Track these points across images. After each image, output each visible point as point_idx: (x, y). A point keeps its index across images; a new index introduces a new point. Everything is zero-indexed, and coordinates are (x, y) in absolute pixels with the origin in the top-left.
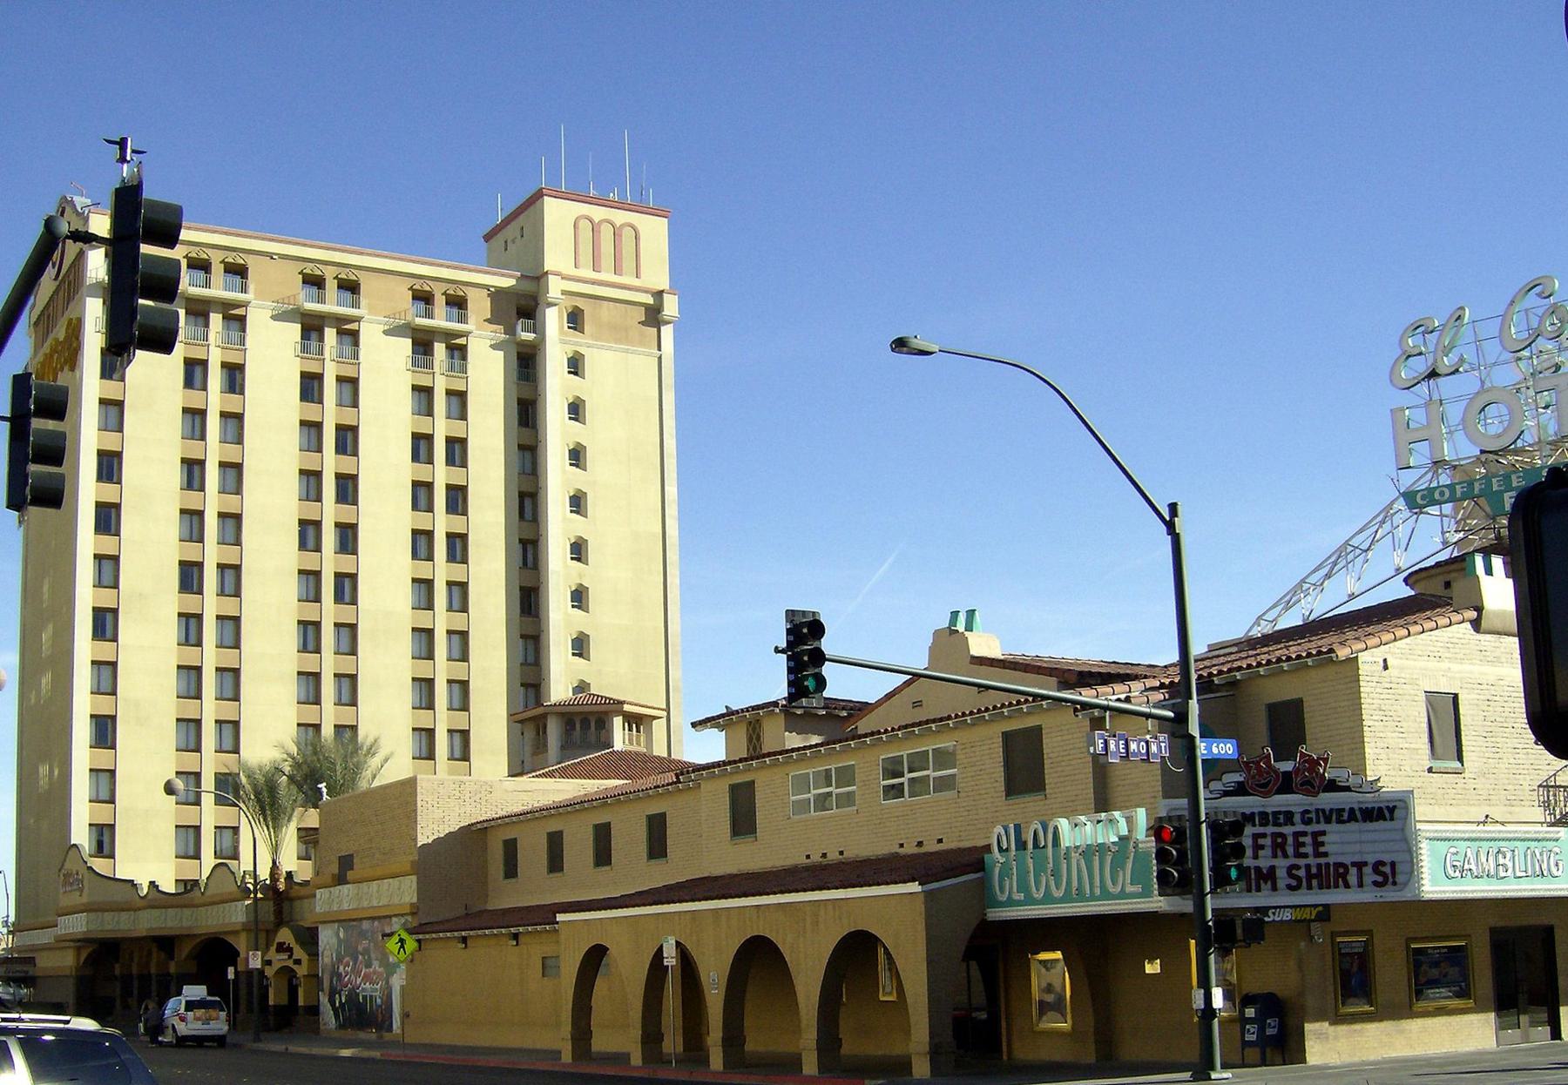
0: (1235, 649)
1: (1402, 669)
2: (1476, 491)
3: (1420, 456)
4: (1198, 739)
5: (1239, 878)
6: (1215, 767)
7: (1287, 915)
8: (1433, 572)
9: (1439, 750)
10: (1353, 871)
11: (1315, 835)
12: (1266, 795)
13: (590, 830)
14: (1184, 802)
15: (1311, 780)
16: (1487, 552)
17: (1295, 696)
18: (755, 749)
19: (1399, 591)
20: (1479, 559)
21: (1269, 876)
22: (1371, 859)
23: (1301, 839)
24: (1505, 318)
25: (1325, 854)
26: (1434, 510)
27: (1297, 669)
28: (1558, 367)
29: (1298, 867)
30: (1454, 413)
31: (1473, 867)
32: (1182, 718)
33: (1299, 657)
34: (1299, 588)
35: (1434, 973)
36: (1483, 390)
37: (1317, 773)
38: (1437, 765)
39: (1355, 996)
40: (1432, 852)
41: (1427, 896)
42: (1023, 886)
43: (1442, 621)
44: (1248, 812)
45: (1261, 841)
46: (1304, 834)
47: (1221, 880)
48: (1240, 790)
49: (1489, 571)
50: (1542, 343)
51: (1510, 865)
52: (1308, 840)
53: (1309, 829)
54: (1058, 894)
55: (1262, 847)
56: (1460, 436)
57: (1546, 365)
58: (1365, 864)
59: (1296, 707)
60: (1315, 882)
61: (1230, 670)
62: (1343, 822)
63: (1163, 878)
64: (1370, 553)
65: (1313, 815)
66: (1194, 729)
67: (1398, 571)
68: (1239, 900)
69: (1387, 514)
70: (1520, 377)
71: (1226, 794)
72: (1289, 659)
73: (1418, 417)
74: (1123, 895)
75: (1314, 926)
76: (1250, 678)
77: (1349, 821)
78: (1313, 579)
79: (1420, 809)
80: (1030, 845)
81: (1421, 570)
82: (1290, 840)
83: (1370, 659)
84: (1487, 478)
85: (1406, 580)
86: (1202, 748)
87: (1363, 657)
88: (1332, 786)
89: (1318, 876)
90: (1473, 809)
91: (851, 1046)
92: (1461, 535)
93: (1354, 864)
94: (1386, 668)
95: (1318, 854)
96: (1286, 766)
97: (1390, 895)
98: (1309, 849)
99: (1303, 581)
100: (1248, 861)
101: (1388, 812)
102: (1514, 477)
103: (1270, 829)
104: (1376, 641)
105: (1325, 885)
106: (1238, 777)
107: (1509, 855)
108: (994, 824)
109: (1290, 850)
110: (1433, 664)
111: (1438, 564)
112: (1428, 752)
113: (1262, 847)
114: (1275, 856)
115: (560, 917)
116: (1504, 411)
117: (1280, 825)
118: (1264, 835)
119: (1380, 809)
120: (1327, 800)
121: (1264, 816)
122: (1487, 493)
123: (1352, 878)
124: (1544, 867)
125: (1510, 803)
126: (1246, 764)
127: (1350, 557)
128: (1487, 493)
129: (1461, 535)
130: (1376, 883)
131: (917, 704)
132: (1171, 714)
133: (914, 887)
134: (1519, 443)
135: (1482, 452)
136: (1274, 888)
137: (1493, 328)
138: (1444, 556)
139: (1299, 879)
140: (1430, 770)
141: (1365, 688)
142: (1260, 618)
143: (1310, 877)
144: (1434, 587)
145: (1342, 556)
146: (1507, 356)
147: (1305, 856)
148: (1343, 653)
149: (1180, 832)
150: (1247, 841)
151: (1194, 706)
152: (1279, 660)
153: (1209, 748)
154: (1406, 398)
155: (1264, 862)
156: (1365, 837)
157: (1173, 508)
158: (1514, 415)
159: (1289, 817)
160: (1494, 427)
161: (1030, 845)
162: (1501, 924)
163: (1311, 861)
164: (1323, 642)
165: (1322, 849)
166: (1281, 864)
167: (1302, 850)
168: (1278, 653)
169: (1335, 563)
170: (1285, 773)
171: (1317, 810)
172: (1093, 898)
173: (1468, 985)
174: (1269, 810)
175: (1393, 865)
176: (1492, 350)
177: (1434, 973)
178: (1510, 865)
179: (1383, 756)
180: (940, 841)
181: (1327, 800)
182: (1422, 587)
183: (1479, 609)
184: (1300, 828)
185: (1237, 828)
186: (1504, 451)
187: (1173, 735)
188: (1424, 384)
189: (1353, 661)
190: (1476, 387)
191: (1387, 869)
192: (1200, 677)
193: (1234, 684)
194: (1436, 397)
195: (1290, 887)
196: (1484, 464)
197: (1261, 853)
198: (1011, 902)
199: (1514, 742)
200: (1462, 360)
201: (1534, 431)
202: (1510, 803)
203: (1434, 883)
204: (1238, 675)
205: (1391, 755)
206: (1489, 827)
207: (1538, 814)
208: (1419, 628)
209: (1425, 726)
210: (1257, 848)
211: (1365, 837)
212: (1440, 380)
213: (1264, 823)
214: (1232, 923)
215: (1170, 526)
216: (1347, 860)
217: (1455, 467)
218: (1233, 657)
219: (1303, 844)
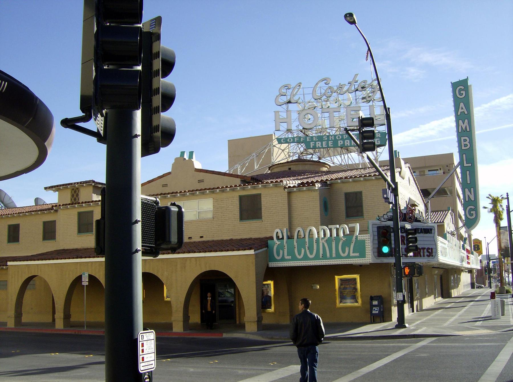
2: (302, 141)
3: (284, 127)
13: (7, 227)
18: (75, 199)
42: (291, 252)
54: (311, 257)
58: (425, 248)
74: (348, 257)
80: (296, 237)
91: (75, 318)
108: (277, 228)
115: (9, 263)
120: (416, 225)
130: (427, 256)
131: (165, 185)
133: (252, 252)
135: (303, 128)
138: (285, 161)
154: (279, 108)
156: (425, 239)
161: (296, 237)
172: (331, 258)
175: (432, 249)
180: (202, 237)
181: (416, 225)
191: (430, 251)
198: (283, 259)
211: (425, 239)
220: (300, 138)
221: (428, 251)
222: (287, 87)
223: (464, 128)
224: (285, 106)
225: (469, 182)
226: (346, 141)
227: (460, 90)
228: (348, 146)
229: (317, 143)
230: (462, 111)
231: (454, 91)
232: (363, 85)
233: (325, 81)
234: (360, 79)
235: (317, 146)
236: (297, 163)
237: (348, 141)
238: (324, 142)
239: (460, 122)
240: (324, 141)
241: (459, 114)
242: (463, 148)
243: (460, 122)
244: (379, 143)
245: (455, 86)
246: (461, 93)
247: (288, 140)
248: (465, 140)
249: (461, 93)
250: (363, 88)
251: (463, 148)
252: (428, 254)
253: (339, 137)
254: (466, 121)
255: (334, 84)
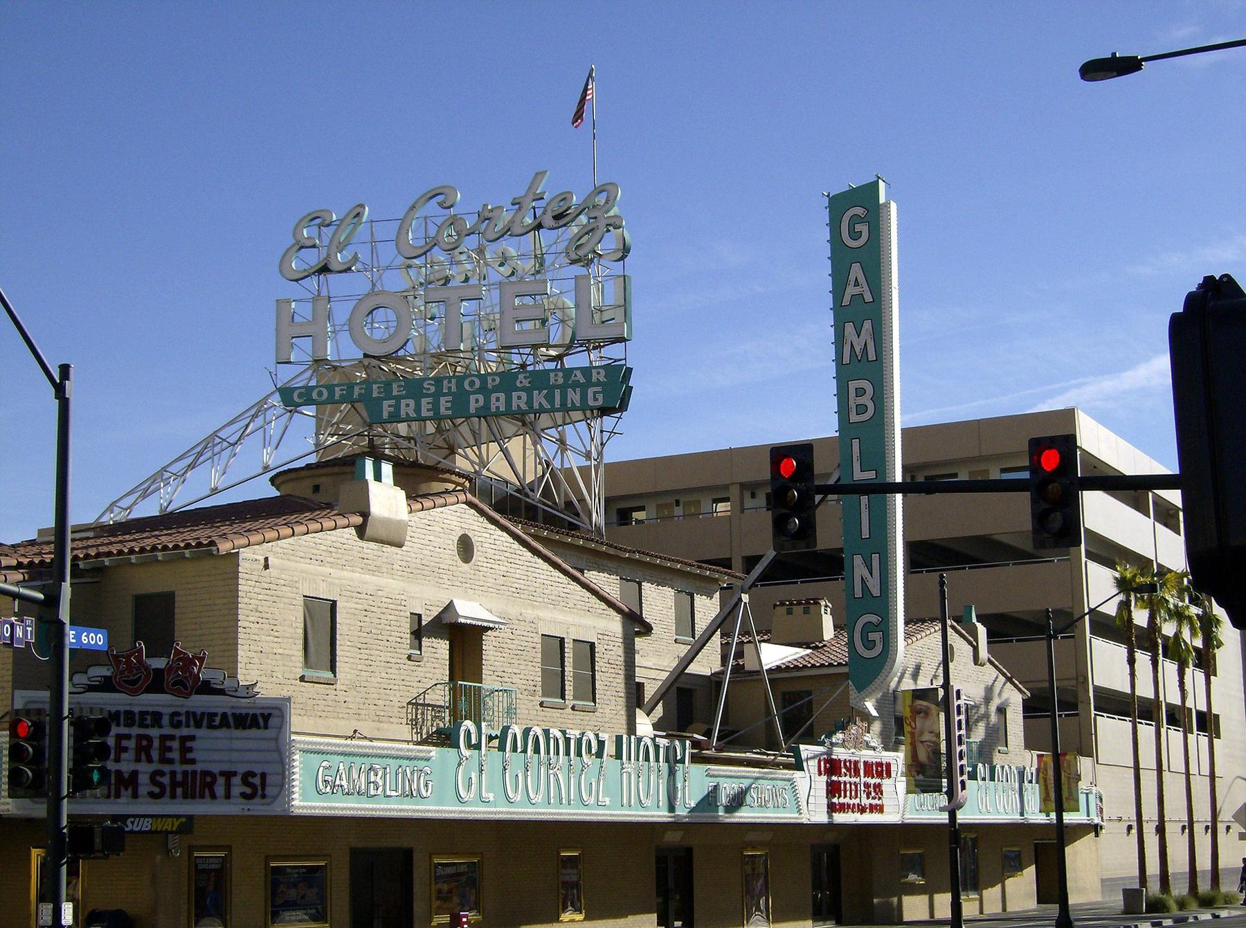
0: (91, 534)
1: (283, 569)
2: (356, 395)
3: (302, 352)
4: (67, 626)
5: (100, 782)
6: (84, 657)
7: (146, 825)
8: (303, 473)
9: (312, 658)
10: (221, 780)
11: (184, 739)
12: (134, 693)
14: (45, 695)
15: (183, 678)
16: (378, 458)
17: (166, 589)
19: (265, 490)
20: (369, 464)
21: (129, 782)
22: (242, 769)
23: (168, 743)
24: (403, 224)
25: (193, 761)
26: (310, 411)
27: (197, 558)
28: (447, 280)
29: (162, 774)
30: (342, 312)
31: (344, 783)
32: (52, 601)
33: (176, 547)
34: (159, 476)
35: (292, 894)
36: (373, 293)
37: (191, 673)
38: (310, 673)
39: (210, 915)
40: (306, 767)
41: (297, 812)
43: (328, 524)
44: (113, 709)
45: (125, 743)
46: (172, 738)
47: (81, 783)
48: (106, 685)
49: (378, 477)
50: (439, 255)
51: (381, 783)
52: (176, 744)
53: (177, 733)
55: (126, 749)
56: (345, 337)
57: (438, 276)
58: (235, 774)
59: (165, 602)
60: (179, 791)
61: (98, 555)
62: (215, 727)
63: (15, 778)
64: (238, 449)
65: (183, 718)
66: (65, 614)
67: (266, 469)
68: (98, 806)
69: (260, 408)
70: (409, 285)
71: (91, 688)
72: (165, 548)
73: (304, 311)
75: (173, 841)
76: (118, 566)
77: (220, 727)
78: (175, 468)
79: (297, 721)
81: (290, 471)
82: (156, 743)
83: (251, 556)
84: (367, 383)
85: (272, 480)
86: (71, 636)
87: (245, 553)
88: (207, 688)
89: (183, 784)
90: (343, 722)
92: (334, 439)
93: (222, 773)
94: (266, 567)
95: (185, 761)
96: (159, 663)
97: (257, 808)
98: (175, 755)
99: (164, 469)
100: (111, 765)
101: (264, 719)
102: (395, 386)
103: (135, 731)
104: (259, 537)
105: (189, 795)
106: (105, 671)
107: (380, 773)
109: (155, 755)
110: (313, 568)
111: (309, 467)
112: (302, 659)
113: (126, 749)
114: (138, 760)
116: (391, 315)
117: (147, 726)
118: (128, 737)
119: (255, 715)
120: (200, 702)
121: (130, 715)
122: (366, 398)
123: (220, 789)
124: (415, 786)
125: (379, 719)
126: (116, 657)
127: (217, 449)
128: (366, 398)
129: (334, 439)
130: (244, 795)
132: (41, 596)
134: (401, 353)
135: (366, 356)
136: (135, 795)
137: (390, 231)
138: (313, 459)
139: (253, 786)
140: (302, 679)
141: (243, 587)
142: (113, 504)
143: (174, 784)
144: (302, 489)
145: (207, 449)
146: (400, 260)
147: (171, 761)
148: (224, 547)
149: (38, 727)
150: (111, 741)
151: (66, 588)
152: (154, 548)
153: (78, 637)
154: (295, 290)
155: (126, 766)
156: (237, 744)
157: (65, 370)
158: (401, 323)
159: (157, 718)
160: (380, 330)
162: (360, 845)
163: (178, 768)
164: (203, 534)
165: (189, 756)
166: (145, 769)
167: (169, 755)
168: (129, 545)
169: (200, 454)
170: (157, 671)
171: (188, 713)
173: (324, 909)
174: (136, 709)
175: (263, 776)
176: (388, 254)
177: (292, 894)
178: (381, 783)
179: (256, 660)
181: (200, 702)
182: (289, 489)
183: (366, 515)
184: (167, 731)
185: (102, 726)
186: (387, 358)
187: (40, 620)
188: (315, 278)
189: (233, 557)
190: (367, 288)
191: (257, 781)
192: (75, 558)
193: (99, 570)
194: (324, 293)
195: (152, 795)
196: (366, 368)
197: (124, 756)
199: (386, 656)
200: (356, 258)
201: (417, 342)
202: (379, 719)
203: (305, 797)
204: (107, 561)
205: (265, 659)
206: (354, 742)
207: (405, 732)
208: (304, 528)
209: (301, 631)
210: (121, 749)
212: (330, 276)
213: (130, 724)
214: (90, 831)
215: (60, 390)
216: (215, 768)
217: (335, 368)
218: (90, 542)
219: (170, 749)
220: (331, 388)
221: (245, 782)
222: (317, 219)
223: (858, 349)
224: (313, 282)
225: (865, 534)
226: (494, 396)
227: (855, 220)
228: (524, 414)
229: (404, 402)
230: (857, 290)
231: (835, 226)
232: (556, 208)
233: (440, 198)
234: (549, 188)
235: (403, 415)
236: (336, 469)
237: (502, 396)
238: (424, 401)
239: (849, 328)
240: (427, 396)
241: (846, 301)
242: (854, 418)
243: (849, 328)
244: (600, 403)
245: (838, 204)
246: (855, 226)
247: (315, 396)
248: (860, 392)
249: (855, 226)
250: (557, 217)
251: (854, 418)
252: (248, 791)
253: (472, 384)
254: (867, 325)
255: (465, 203)
